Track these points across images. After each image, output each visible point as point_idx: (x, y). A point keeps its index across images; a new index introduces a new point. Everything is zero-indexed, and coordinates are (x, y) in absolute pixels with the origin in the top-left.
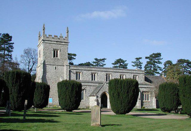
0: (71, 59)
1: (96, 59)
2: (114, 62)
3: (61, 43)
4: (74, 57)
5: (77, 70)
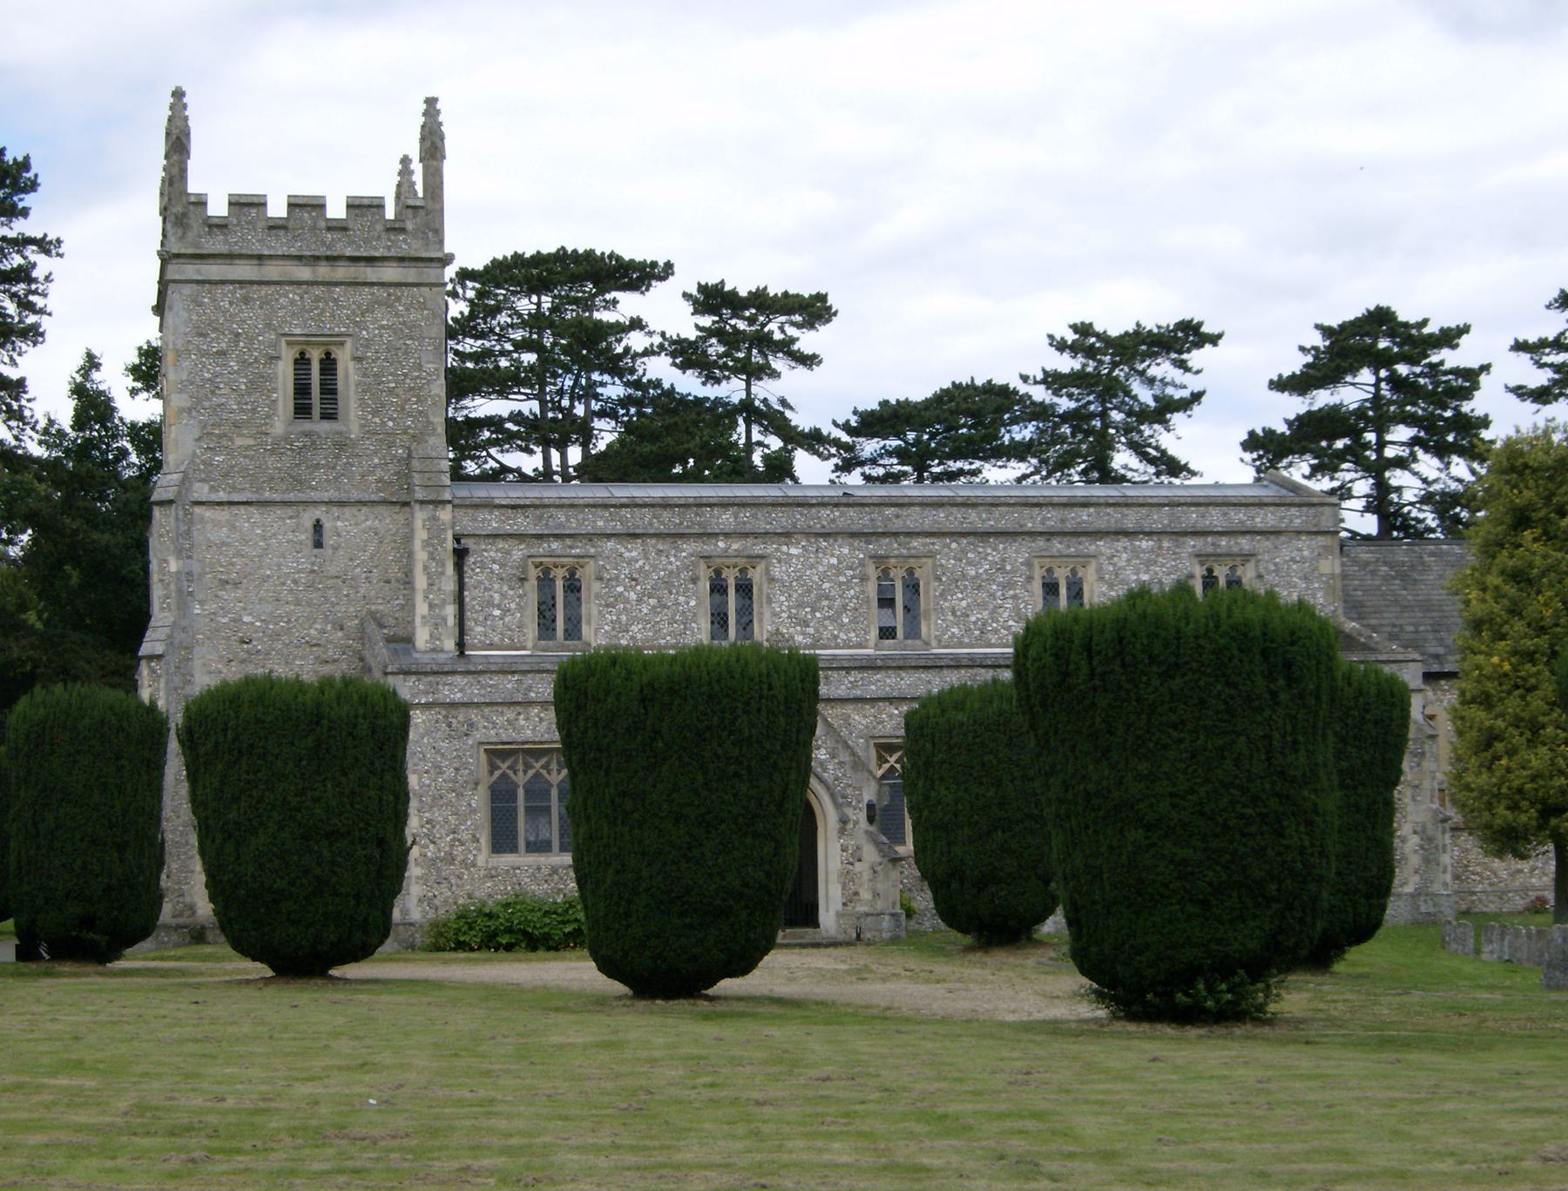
0: (765, 371)
1: (1084, 340)
2: (1295, 364)
3: (370, 273)
4: (807, 341)
5: (540, 537)
